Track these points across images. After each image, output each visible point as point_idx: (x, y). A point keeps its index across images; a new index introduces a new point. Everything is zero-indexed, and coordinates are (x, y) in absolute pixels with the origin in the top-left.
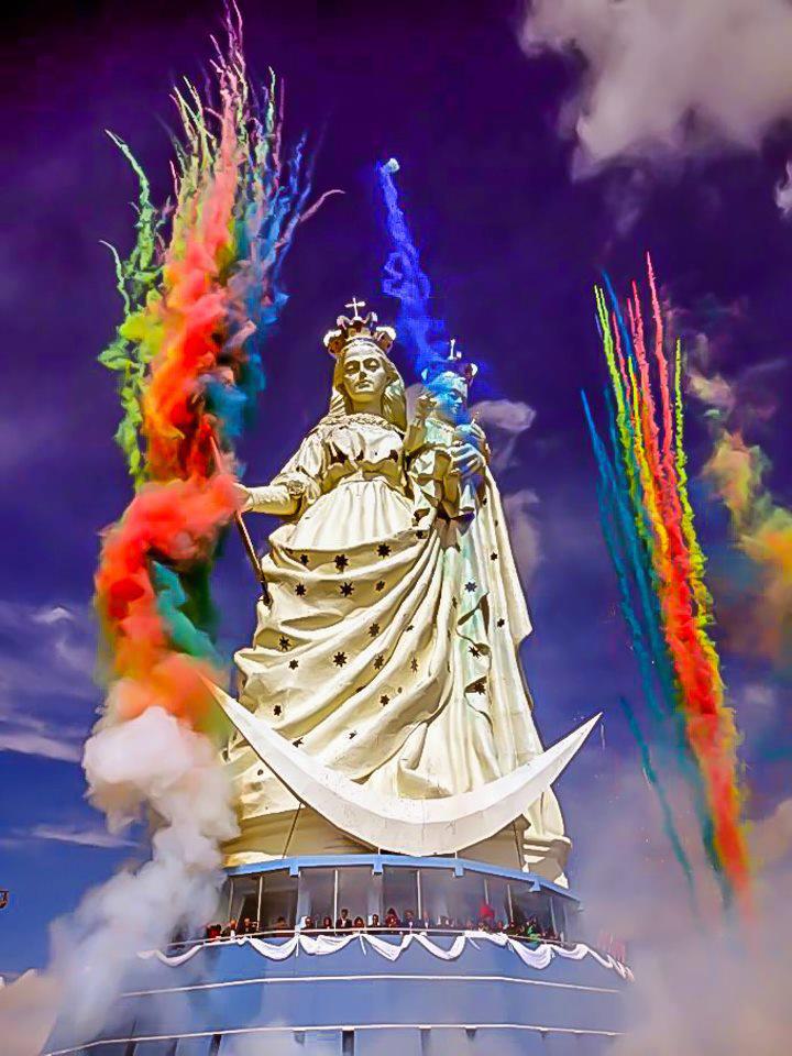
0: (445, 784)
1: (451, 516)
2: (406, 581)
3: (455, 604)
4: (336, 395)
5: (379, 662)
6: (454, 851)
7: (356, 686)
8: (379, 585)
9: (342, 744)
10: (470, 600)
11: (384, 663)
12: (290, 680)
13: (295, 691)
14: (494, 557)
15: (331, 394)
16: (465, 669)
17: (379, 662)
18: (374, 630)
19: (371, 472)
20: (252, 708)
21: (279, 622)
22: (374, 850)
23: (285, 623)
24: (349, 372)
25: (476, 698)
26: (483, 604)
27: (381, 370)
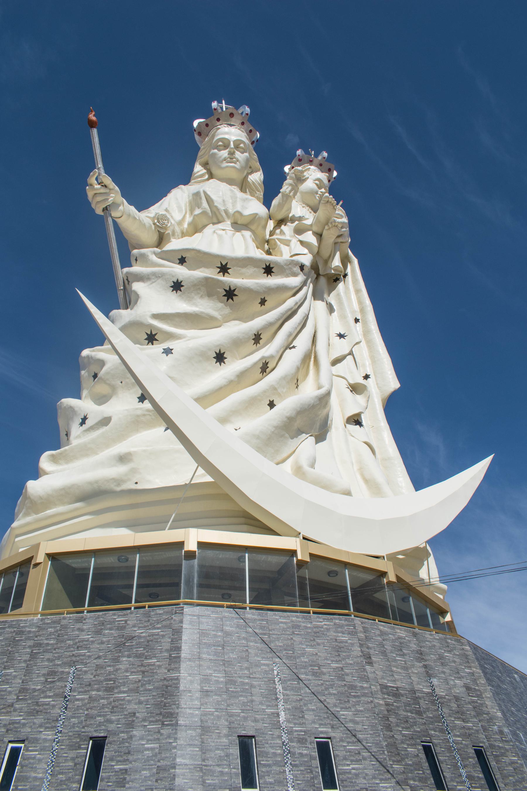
1: (321, 272)
2: (290, 303)
11: (268, 370)
14: (357, 320)
17: (265, 368)
18: (257, 338)
21: (150, 314)
23: (156, 316)
24: (217, 147)
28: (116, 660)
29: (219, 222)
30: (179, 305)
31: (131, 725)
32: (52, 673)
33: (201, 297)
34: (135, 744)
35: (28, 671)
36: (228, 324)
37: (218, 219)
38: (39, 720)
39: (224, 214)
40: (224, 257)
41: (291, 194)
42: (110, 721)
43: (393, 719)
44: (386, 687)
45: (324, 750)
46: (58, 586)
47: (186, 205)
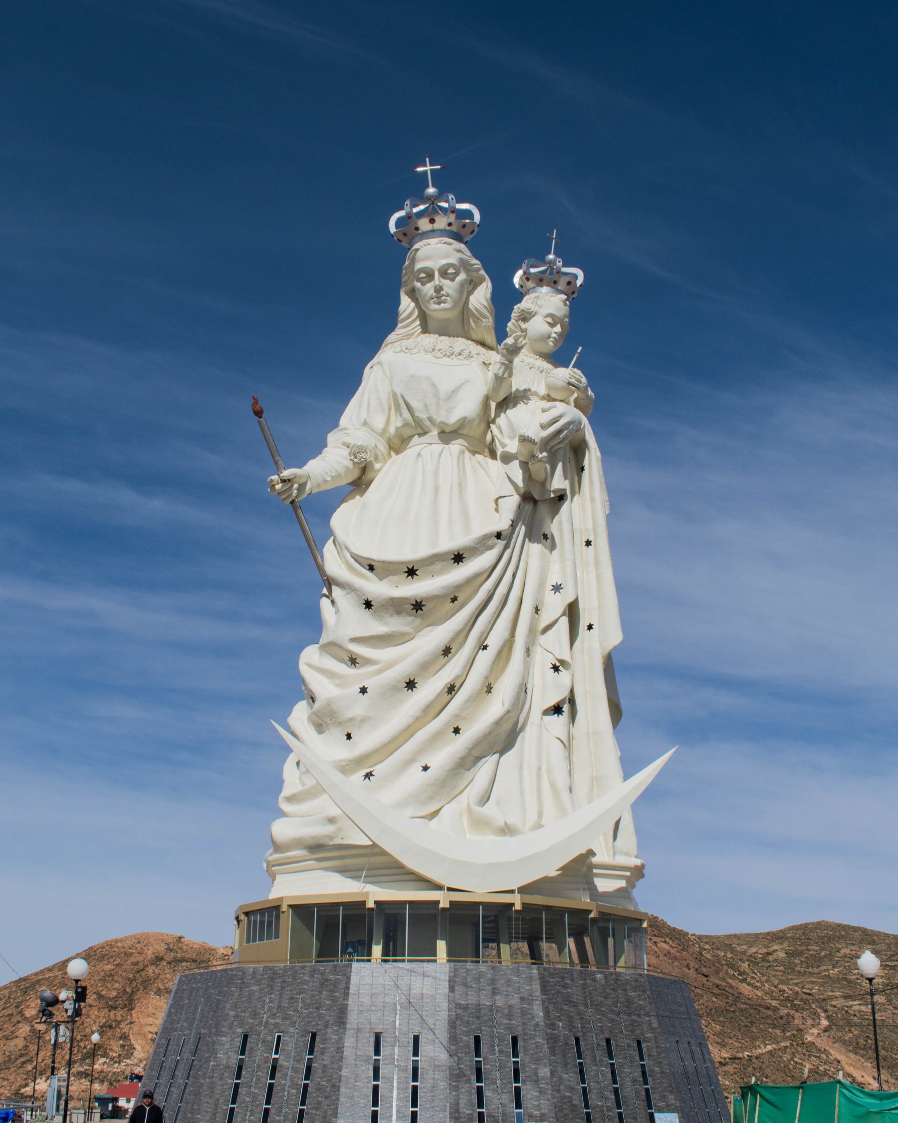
0: (513, 820)
3: (537, 610)
4: (406, 304)
5: (451, 689)
6: (515, 887)
7: (432, 710)
8: (454, 598)
9: (415, 777)
10: (555, 606)
12: (359, 707)
13: (364, 720)
14: (588, 543)
15: (398, 303)
16: (547, 689)
17: (451, 689)
18: (447, 651)
19: (447, 435)
20: (320, 728)
21: (347, 638)
22: (439, 887)
23: (354, 640)
25: (559, 722)
26: (572, 611)
27: (462, 276)
28: (321, 992)
29: (425, 433)
30: (375, 626)
31: (327, 1027)
32: (291, 998)
33: (391, 615)
34: (328, 1036)
35: (281, 996)
36: (421, 633)
37: (423, 429)
38: (288, 1022)
39: (428, 423)
40: (409, 562)
41: (506, 375)
42: (318, 1024)
43: (458, 1023)
44: (460, 1004)
45: (416, 1039)
46: (299, 923)
47: (389, 398)
